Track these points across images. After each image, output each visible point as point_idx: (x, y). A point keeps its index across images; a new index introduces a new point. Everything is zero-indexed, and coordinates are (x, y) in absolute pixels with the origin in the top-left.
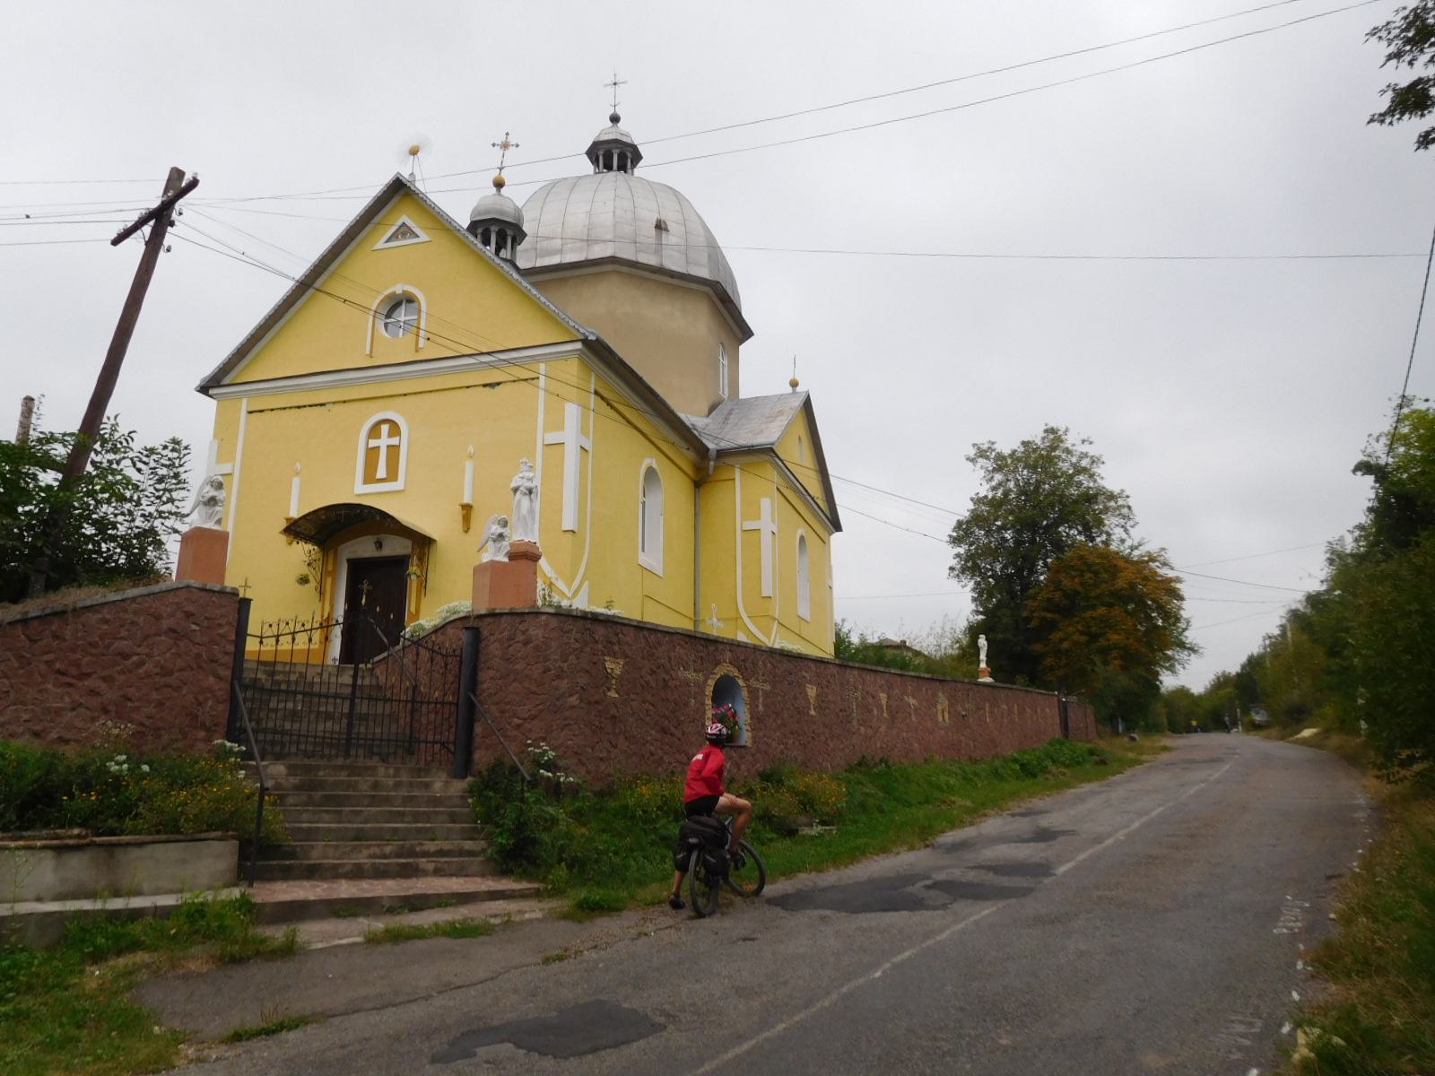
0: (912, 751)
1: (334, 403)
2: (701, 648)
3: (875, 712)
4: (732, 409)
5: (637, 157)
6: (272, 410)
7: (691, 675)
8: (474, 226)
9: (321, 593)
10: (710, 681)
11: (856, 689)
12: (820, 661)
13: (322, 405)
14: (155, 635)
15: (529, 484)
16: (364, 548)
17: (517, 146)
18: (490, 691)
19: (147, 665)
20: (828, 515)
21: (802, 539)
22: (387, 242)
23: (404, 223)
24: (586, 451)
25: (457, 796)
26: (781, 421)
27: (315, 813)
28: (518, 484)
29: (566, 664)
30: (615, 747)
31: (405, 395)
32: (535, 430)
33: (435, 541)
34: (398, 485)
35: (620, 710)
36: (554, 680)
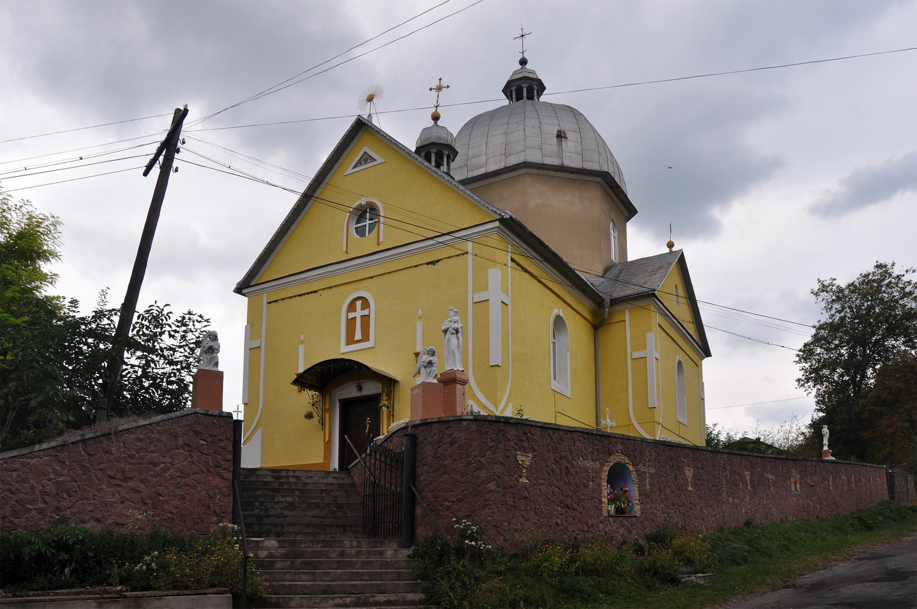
0: (771, 514)
1: (323, 289)
2: (597, 442)
3: (741, 486)
4: (622, 270)
5: (542, 88)
6: (283, 299)
7: (589, 464)
8: (418, 150)
9: (323, 424)
10: (605, 468)
11: (726, 469)
12: (695, 449)
13: (315, 292)
14: (174, 449)
15: (456, 326)
16: (350, 392)
17: (448, 87)
18: (426, 482)
19: (171, 470)
20: (700, 344)
21: (680, 363)
22: (353, 168)
23: (365, 152)
24: (506, 305)
25: (403, 561)
26: (661, 273)
27: (295, 574)
28: (448, 326)
29: (484, 458)
30: (527, 520)
31: (372, 278)
32: (466, 292)
33: (398, 381)
34: (370, 344)
35: (531, 493)
36: (475, 472)
